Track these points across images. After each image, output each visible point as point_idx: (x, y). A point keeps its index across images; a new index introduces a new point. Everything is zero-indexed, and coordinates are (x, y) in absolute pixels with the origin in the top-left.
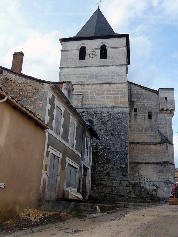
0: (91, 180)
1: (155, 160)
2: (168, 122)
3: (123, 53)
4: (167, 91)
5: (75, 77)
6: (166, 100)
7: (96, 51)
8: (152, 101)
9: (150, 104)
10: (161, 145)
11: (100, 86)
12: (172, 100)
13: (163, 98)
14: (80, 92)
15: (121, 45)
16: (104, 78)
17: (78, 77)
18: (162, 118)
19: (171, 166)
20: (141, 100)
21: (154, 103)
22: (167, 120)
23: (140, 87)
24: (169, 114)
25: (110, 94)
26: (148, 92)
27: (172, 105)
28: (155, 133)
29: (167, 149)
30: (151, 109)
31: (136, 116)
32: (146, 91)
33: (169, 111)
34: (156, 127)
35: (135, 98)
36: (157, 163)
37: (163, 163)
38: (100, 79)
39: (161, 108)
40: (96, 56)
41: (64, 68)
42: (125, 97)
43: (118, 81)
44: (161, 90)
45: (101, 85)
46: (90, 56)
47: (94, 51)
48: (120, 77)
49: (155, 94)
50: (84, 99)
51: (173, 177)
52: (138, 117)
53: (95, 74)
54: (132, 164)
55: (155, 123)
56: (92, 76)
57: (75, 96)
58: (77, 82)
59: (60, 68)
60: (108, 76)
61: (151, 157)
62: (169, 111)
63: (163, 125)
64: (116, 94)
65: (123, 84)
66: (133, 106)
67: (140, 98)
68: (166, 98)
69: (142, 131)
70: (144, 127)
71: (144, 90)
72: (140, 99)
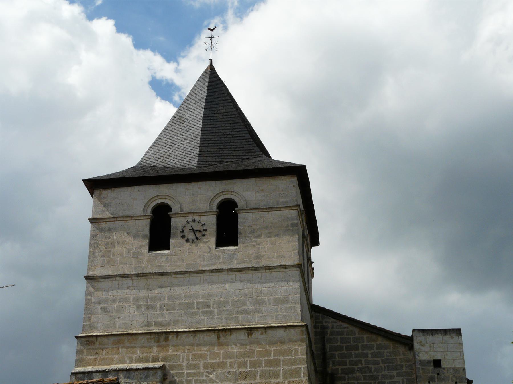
3: (288, 226)
5: (138, 307)
6: (437, 369)
7: (204, 219)
8: (394, 373)
11: (219, 338)
13: (429, 362)
14: (155, 360)
15: (281, 200)
16: (229, 312)
17: (148, 307)
25: (253, 364)
26: (380, 341)
32: (374, 336)
38: (220, 313)
40: (204, 235)
41: (102, 277)
42: (297, 372)
45: (221, 334)
46: (183, 237)
47: (197, 218)
48: (280, 306)
49: (401, 349)
53: (203, 297)
56: (192, 304)
57: (136, 373)
58: (146, 326)
59: (87, 278)
60: (244, 304)
64: (270, 363)
65: (292, 330)
67: (356, 363)
68: (437, 363)
71: (366, 336)
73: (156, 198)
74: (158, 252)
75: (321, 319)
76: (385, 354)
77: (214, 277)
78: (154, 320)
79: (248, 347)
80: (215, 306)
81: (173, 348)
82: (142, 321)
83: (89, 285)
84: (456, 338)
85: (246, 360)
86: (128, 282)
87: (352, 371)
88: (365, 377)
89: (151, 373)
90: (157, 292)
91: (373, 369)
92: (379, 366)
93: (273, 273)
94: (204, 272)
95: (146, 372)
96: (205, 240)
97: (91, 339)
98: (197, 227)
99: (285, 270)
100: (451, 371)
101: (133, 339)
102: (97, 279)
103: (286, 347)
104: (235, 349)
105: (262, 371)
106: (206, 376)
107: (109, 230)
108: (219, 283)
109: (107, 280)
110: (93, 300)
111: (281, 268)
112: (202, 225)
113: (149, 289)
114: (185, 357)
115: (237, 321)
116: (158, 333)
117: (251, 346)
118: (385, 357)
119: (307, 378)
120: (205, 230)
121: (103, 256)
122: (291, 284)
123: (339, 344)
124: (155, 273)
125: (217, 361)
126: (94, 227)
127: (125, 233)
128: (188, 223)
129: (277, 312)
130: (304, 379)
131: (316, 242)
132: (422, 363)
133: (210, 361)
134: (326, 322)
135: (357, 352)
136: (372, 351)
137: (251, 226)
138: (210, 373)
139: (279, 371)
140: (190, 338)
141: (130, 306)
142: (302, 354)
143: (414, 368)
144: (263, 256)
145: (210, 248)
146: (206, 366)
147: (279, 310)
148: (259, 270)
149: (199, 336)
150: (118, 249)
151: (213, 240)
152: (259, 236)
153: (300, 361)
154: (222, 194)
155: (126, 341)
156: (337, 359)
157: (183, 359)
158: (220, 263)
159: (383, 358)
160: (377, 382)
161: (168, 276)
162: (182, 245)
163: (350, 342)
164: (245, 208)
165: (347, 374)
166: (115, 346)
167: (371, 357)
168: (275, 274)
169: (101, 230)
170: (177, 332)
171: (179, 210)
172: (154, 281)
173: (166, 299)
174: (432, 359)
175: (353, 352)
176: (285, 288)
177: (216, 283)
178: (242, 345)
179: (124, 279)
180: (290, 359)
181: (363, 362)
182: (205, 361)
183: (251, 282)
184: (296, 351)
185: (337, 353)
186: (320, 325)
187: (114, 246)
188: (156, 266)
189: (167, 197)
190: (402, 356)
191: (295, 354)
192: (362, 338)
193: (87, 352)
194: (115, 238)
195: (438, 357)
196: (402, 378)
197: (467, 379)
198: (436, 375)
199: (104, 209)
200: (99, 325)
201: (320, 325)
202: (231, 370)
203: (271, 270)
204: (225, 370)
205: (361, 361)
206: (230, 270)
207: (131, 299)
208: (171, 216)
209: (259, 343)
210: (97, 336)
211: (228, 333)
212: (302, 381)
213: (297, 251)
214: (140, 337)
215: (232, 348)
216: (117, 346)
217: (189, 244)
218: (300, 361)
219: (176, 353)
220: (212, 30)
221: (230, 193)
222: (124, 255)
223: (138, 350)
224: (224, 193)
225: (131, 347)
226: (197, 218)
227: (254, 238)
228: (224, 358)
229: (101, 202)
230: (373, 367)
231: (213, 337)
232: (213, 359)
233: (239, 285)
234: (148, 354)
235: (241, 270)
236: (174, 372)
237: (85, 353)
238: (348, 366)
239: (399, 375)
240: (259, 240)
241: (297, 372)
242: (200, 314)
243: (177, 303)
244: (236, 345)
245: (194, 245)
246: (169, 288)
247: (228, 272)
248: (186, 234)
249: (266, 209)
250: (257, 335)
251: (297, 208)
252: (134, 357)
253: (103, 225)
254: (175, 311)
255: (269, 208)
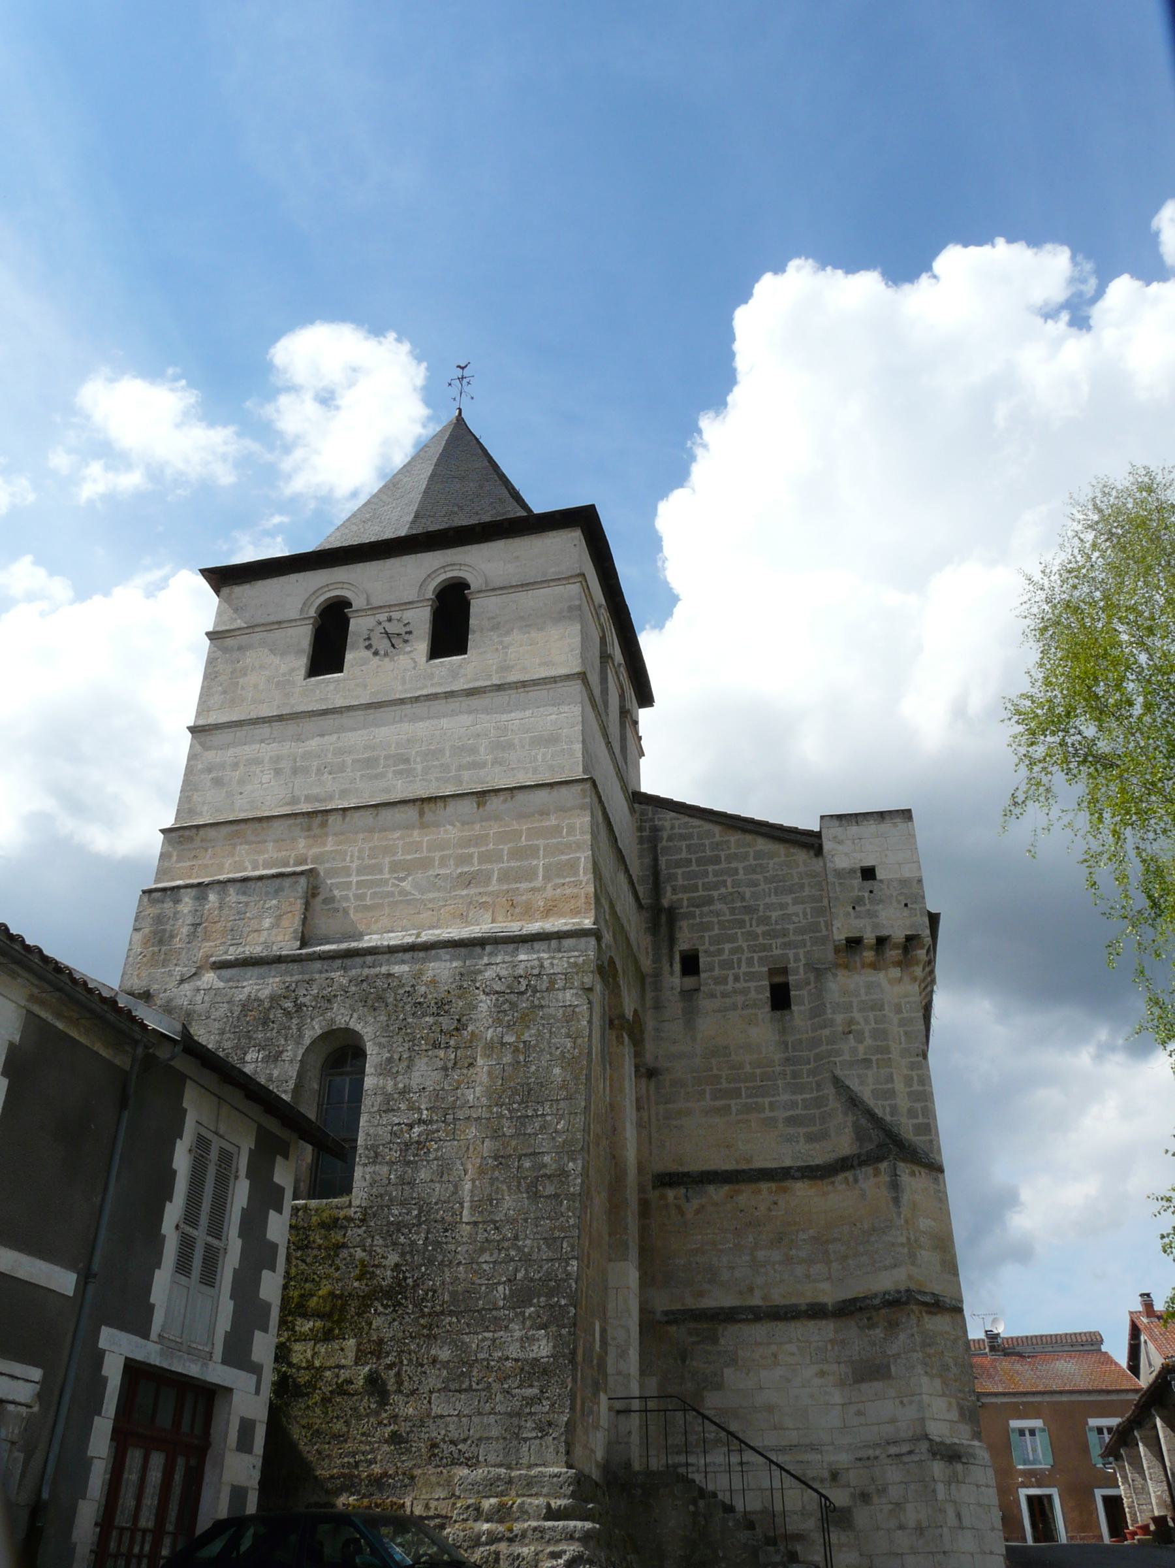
0: (262, 1483)
1: (825, 1286)
2: (895, 1019)
4: (871, 828)
5: (278, 772)
7: (409, 615)
8: (788, 899)
9: (774, 915)
10: (856, 1181)
11: (421, 814)
12: (904, 882)
17: (295, 771)
18: (855, 1001)
19: (938, 1324)
20: (723, 898)
21: (798, 909)
22: (888, 1011)
23: (705, 820)
24: (895, 972)
25: (485, 858)
26: (762, 844)
27: (906, 912)
28: (819, 1102)
29: (897, 1201)
30: (786, 945)
31: (689, 995)
32: (749, 838)
33: (896, 946)
34: (818, 1057)
35: (685, 889)
36: (848, 1310)
37: (877, 1308)
38: (426, 770)
39: (841, 931)
40: (406, 641)
42: (572, 866)
43: (535, 770)
44: (836, 823)
45: (426, 807)
46: (368, 647)
47: (395, 615)
49: (801, 856)
50: (319, 899)
51: (961, 1409)
52: (705, 1004)
54: (673, 1329)
55: (811, 1034)
56: (377, 759)
57: (260, 884)
58: (288, 804)
59: (192, 729)
60: (473, 750)
61: (800, 1270)
62: (896, 946)
63: (861, 1042)
64: (516, 854)
65: (564, 790)
66: (672, 940)
67: (716, 886)
68: (868, 873)
69: (736, 1093)
70: (748, 1069)
71: (734, 838)
72: (715, 894)
73: (326, 589)
74: (322, 677)
75: (650, 816)
76: (771, 866)
77: (419, 709)
78: (306, 793)
79: (477, 827)
80: (418, 759)
81: (335, 838)
82: (281, 796)
83: (195, 741)
84: (902, 826)
85: (472, 850)
86: (265, 730)
87: (709, 901)
88: (733, 911)
89: (287, 882)
90: (313, 744)
91: (748, 895)
92: (760, 888)
93: (530, 694)
94: (402, 701)
95: (278, 881)
96: (408, 649)
97: (187, 833)
98: (392, 628)
99: (553, 686)
100: (895, 884)
101: (263, 829)
102: (210, 730)
103: (553, 821)
104: (451, 833)
105: (501, 868)
106: (394, 885)
107: (240, 648)
108: (429, 718)
109: (227, 730)
110: (200, 766)
111: (546, 684)
112: (405, 625)
113: (299, 739)
114: (356, 854)
115: (460, 782)
116: (308, 813)
117: (484, 824)
118: (771, 872)
119: (592, 876)
120: (410, 633)
121: (225, 692)
122: (566, 708)
123: (684, 855)
124: (313, 711)
125: (417, 855)
126: (215, 646)
127: (266, 651)
128: (380, 623)
129: (535, 760)
130: (585, 879)
131: (645, 698)
132: (839, 874)
133: (403, 858)
134: (660, 819)
135: (717, 867)
136: (747, 863)
137: (493, 618)
138: (402, 879)
139: (537, 866)
140: (367, 818)
141: (262, 772)
142: (582, 833)
143: (825, 888)
144: (512, 667)
145: (415, 662)
146: (395, 867)
147: (539, 757)
148: (504, 690)
149: (387, 814)
150: (252, 678)
151: (422, 647)
152: (508, 633)
153: (579, 846)
154: (442, 570)
155: (249, 832)
156: (680, 882)
157: (352, 856)
158: (432, 685)
159: (767, 875)
160: (755, 916)
161: (336, 716)
162: (365, 662)
163: (704, 851)
164: (484, 588)
165: (698, 906)
166: (229, 842)
167: (745, 874)
168: (534, 694)
169: (225, 650)
170: (345, 810)
171: (365, 603)
172: (310, 725)
173: (330, 756)
174: (858, 866)
175: (710, 868)
176: (554, 717)
177: (422, 719)
178: (463, 824)
179: (257, 726)
180: (558, 843)
181: (729, 883)
182: (392, 858)
183: (487, 711)
184: (571, 829)
185: (680, 871)
186: (647, 825)
187: (245, 675)
188: (316, 701)
189: (345, 586)
190: (801, 869)
191: (569, 834)
192: (728, 841)
193: (178, 856)
194: (248, 660)
195: (868, 863)
196: (803, 906)
197: (929, 912)
198: (866, 894)
199: (235, 616)
200: (206, 808)
201: (647, 825)
202: (441, 872)
203: (527, 689)
204: (431, 873)
205: (725, 881)
206: (450, 695)
207: (267, 759)
208: (350, 615)
209: (497, 818)
210: (198, 827)
211: (440, 804)
212: (581, 882)
213: (578, 651)
214: (276, 824)
215: (446, 831)
216: (232, 842)
217: (378, 657)
218: (579, 846)
219: (340, 847)
220: (463, 368)
221: (458, 567)
222: (261, 687)
223: (270, 846)
224: (447, 569)
225: (259, 842)
226: (395, 615)
227: (498, 637)
228: (429, 851)
229: (230, 605)
230: (748, 892)
231: (411, 813)
232: (409, 854)
233: (466, 719)
234: (288, 853)
235: (471, 693)
236: (333, 881)
237: (175, 858)
238: (701, 893)
239: (796, 902)
240: (507, 639)
241: (572, 866)
242: (390, 775)
243: (349, 760)
244: (454, 826)
245: (387, 660)
246: (335, 736)
247: (446, 698)
248: (374, 642)
249: (522, 585)
250: (494, 803)
251: (580, 579)
252: (261, 859)
253: (229, 642)
254: (344, 774)
255: (527, 584)
